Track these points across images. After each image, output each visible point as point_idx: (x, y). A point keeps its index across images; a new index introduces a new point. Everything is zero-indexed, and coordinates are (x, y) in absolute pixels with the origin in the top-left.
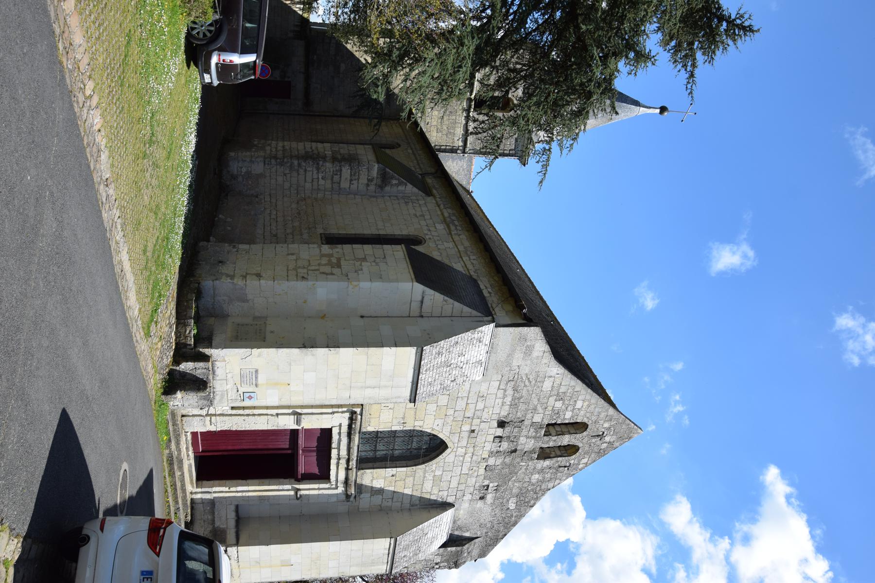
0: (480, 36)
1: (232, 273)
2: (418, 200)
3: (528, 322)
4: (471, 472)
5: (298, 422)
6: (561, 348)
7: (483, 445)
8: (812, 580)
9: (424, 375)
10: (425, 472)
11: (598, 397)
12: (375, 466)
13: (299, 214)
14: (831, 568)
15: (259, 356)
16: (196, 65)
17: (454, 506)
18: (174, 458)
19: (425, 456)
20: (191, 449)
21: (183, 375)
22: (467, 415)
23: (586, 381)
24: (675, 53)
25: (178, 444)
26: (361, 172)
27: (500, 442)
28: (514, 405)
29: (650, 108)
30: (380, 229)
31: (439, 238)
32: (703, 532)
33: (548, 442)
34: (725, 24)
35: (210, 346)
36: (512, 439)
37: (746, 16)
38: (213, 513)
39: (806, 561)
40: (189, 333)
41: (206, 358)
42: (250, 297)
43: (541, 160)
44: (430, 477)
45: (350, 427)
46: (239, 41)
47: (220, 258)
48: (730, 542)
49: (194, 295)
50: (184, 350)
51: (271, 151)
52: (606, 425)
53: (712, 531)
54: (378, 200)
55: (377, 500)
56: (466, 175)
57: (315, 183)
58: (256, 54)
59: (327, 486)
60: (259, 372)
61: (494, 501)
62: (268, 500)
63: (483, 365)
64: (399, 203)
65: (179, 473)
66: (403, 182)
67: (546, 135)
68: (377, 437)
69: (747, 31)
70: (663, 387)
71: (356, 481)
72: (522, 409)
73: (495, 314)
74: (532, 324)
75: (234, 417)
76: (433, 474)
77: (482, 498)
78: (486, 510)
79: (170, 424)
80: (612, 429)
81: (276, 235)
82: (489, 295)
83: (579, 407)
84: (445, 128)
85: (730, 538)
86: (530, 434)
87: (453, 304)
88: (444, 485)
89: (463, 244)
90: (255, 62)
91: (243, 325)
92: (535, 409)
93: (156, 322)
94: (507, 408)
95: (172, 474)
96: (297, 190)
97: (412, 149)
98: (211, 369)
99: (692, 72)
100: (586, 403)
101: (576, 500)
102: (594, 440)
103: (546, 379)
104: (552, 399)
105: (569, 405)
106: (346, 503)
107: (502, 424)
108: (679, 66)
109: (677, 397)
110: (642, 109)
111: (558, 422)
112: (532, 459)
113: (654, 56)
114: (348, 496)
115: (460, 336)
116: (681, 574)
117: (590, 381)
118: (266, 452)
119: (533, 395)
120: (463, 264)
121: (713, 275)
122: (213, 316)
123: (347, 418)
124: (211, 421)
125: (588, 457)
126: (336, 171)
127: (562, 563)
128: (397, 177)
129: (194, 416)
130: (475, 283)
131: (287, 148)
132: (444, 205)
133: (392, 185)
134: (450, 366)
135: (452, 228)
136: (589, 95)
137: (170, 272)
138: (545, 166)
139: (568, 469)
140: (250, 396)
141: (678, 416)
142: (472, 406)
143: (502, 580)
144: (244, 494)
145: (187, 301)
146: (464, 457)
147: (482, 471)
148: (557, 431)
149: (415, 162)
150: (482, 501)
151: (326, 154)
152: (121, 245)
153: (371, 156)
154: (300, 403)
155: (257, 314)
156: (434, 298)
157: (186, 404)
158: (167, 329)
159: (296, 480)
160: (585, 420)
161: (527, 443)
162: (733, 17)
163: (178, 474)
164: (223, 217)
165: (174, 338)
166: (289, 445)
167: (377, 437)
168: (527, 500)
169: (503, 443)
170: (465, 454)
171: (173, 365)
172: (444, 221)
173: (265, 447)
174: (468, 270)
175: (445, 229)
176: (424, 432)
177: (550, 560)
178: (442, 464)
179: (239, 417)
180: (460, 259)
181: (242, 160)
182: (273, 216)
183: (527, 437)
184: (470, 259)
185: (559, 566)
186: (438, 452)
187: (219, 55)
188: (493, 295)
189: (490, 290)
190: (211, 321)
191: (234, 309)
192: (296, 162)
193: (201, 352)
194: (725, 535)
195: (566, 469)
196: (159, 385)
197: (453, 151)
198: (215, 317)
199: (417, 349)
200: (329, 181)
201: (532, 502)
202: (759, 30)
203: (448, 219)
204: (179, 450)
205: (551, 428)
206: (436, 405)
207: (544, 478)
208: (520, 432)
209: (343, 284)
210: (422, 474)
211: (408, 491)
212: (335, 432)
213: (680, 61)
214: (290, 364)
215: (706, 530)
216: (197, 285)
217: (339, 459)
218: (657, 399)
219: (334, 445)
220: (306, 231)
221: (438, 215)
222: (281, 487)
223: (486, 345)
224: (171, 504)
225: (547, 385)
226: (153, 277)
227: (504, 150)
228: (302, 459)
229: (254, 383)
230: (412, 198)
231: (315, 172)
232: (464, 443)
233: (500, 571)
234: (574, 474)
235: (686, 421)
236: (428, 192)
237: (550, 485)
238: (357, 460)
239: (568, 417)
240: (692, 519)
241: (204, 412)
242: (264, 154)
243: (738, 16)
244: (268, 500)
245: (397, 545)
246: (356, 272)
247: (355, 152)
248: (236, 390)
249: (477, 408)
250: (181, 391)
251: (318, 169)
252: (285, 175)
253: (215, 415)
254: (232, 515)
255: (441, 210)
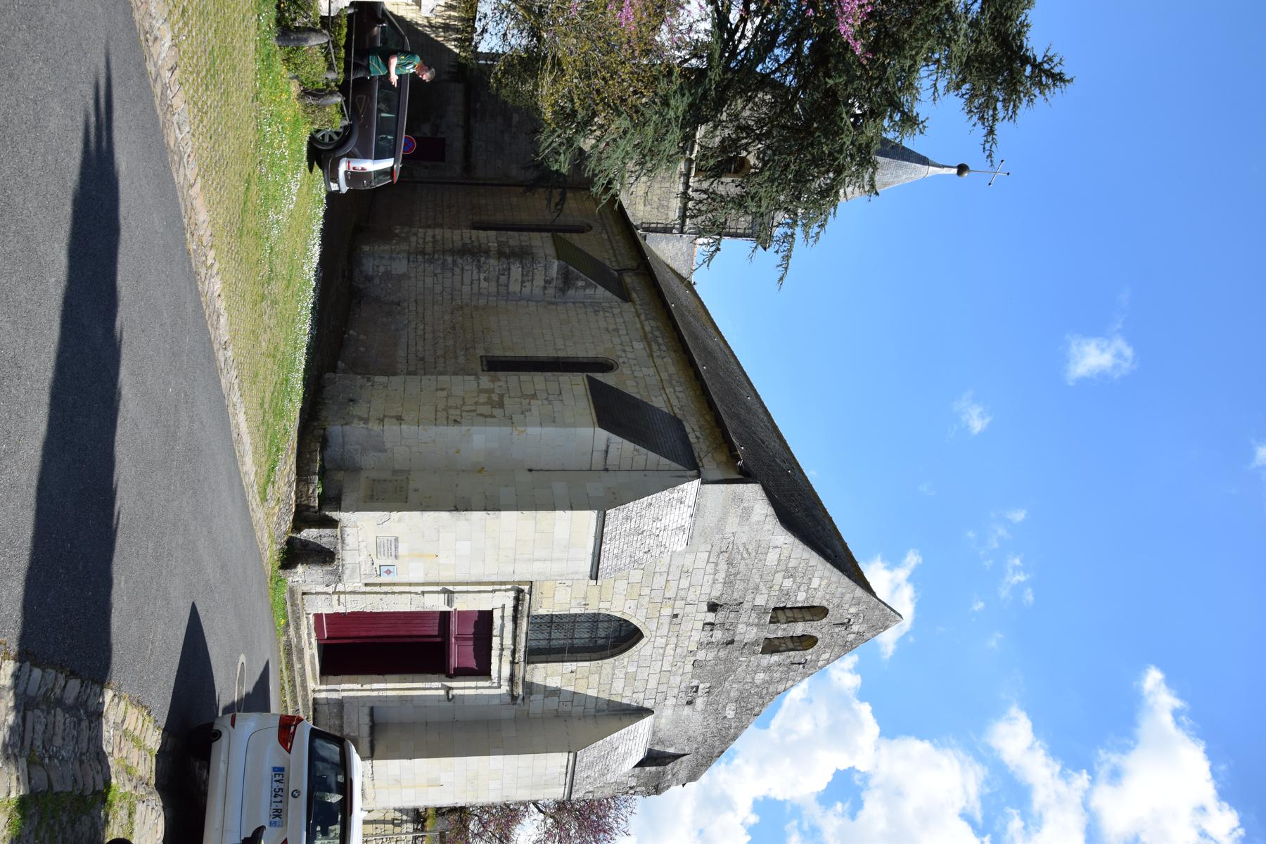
0: (693, 91)
1: (366, 416)
2: (611, 308)
3: (746, 476)
4: (674, 669)
5: (449, 603)
6: (797, 507)
7: (689, 634)
8: (1212, 839)
9: (608, 546)
10: (614, 668)
11: (841, 574)
12: (549, 659)
13: (453, 328)
14: (1243, 823)
15: (400, 520)
16: (321, 167)
17: (653, 712)
18: (293, 646)
19: (614, 647)
20: (314, 634)
21: (305, 544)
22: (667, 595)
23: (829, 551)
24: (970, 100)
25: (298, 628)
26: (536, 271)
27: (711, 630)
28: (728, 583)
29: (944, 166)
30: (560, 350)
31: (635, 361)
32: (1051, 762)
33: (775, 631)
34: (1028, 69)
35: (338, 508)
36: (727, 626)
37: (1056, 60)
38: (342, 718)
39: (1202, 809)
40: (313, 492)
41: (333, 524)
42: (388, 445)
43: (781, 249)
44: (620, 674)
45: (516, 609)
46: (372, 143)
47: (351, 395)
48: (1090, 778)
49: (318, 445)
50: (306, 513)
51: (418, 243)
52: (853, 610)
53: (1063, 762)
54: (559, 308)
55: (552, 703)
56: (686, 261)
57: (475, 286)
58: (393, 159)
59: (487, 684)
60: (400, 540)
61: (706, 707)
62: (412, 700)
63: (687, 532)
64: (586, 313)
65: (299, 666)
66: (591, 284)
67: (786, 216)
68: (551, 622)
69: (1057, 80)
70: (996, 545)
71: (524, 678)
72: (740, 587)
73: (703, 466)
74: (750, 480)
75: (368, 596)
76: (624, 671)
77: (689, 703)
78: (695, 720)
79: (289, 604)
80: (861, 615)
81: (422, 359)
82: (696, 440)
83: (816, 586)
84: (655, 199)
85: (1091, 772)
86: (751, 620)
87: (647, 454)
88: (640, 685)
89: (667, 371)
90: (392, 167)
91: (379, 481)
92: (757, 588)
93: (273, 483)
94: (719, 586)
95: (290, 666)
96: (452, 294)
97: (607, 233)
98: (339, 536)
99: (991, 127)
100: (825, 581)
101: (865, 710)
102: (837, 630)
103: (770, 550)
104: (779, 577)
105: (801, 584)
106: (511, 706)
107: (713, 607)
108: (975, 118)
109: (1017, 562)
110: (931, 168)
111: (788, 606)
112: (754, 653)
113: (922, 122)
114: (514, 698)
115: (655, 495)
116: (1016, 824)
117: (834, 552)
118: (409, 640)
119: (754, 571)
120: (666, 399)
121: (1071, 384)
122: (341, 470)
123: (512, 598)
124: (339, 600)
125: (830, 651)
126: (503, 269)
127: (843, 802)
128: (584, 277)
129: (317, 593)
130: (678, 423)
131: (439, 237)
132: (646, 315)
133: (577, 288)
134: (642, 533)
135: (655, 347)
136: (839, 171)
137: (289, 420)
138: (787, 257)
139: (804, 667)
140: (388, 570)
141: (1018, 589)
142: (673, 585)
143: (755, 825)
144: (381, 693)
145: (310, 453)
146: (664, 648)
147: (689, 668)
148: (787, 617)
149: (611, 251)
150: (690, 706)
151: (489, 247)
152: (238, 406)
153: (550, 250)
154: (452, 580)
155: (397, 467)
156: (622, 448)
157: (309, 580)
158: (285, 489)
159: (447, 676)
160: (825, 604)
161: (748, 632)
162: (1039, 60)
163: (297, 666)
164: (355, 334)
165: (294, 499)
166: (439, 631)
167: (551, 622)
168: (750, 706)
169: (715, 632)
170: (667, 645)
171: (292, 532)
172: (645, 338)
173: (408, 633)
174: (671, 406)
175: (645, 349)
176: (612, 616)
177: (827, 798)
178: (635, 658)
179: (375, 595)
180: (663, 391)
181: (379, 257)
182: (420, 332)
183: (748, 625)
184: (675, 391)
185: (839, 806)
186: (631, 642)
187: (349, 162)
188: (701, 440)
189: (698, 434)
190: (340, 475)
191: (368, 460)
192: (450, 259)
193: (327, 516)
194: (1082, 769)
195: (801, 666)
196: (276, 557)
197: (667, 230)
198: (345, 471)
199: (599, 513)
200: (494, 284)
201: (757, 709)
202: (1072, 79)
203: (650, 336)
204: (299, 637)
205: (780, 612)
206: (626, 582)
207: (772, 678)
208: (737, 618)
209: (506, 430)
210: (609, 670)
211: (592, 693)
212: (497, 615)
213: (976, 111)
214: (439, 531)
215: (1054, 760)
216: (322, 431)
217: (502, 649)
218: (986, 564)
219: (496, 632)
220: (462, 353)
221: (637, 329)
222: (428, 685)
223: (689, 507)
224: (288, 704)
225: (772, 557)
226: (270, 431)
227: (737, 229)
228: (454, 649)
229: (393, 554)
230: (603, 304)
231: (475, 272)
232: (664, 631)
233: (752, 812)
234: (812, 674)
235: (1029, 596)
236: (625, 296)
237: (781, 688)
238: (525, 652)
239: (801, 599)
240: (1033, 743)
241: (330, 589)
242: (407, 248)
243: (1045, 59)
244: (412, 700)
245: (577, 763)
246: (522, 413)
247: (527, 244)
248: (371, 563)
249: (680, 587)
250: (302, 564)
251: (479, 267)
252: (435, 275)
253: (344, 593)
254: (366, 720)
255: (641, 323)
